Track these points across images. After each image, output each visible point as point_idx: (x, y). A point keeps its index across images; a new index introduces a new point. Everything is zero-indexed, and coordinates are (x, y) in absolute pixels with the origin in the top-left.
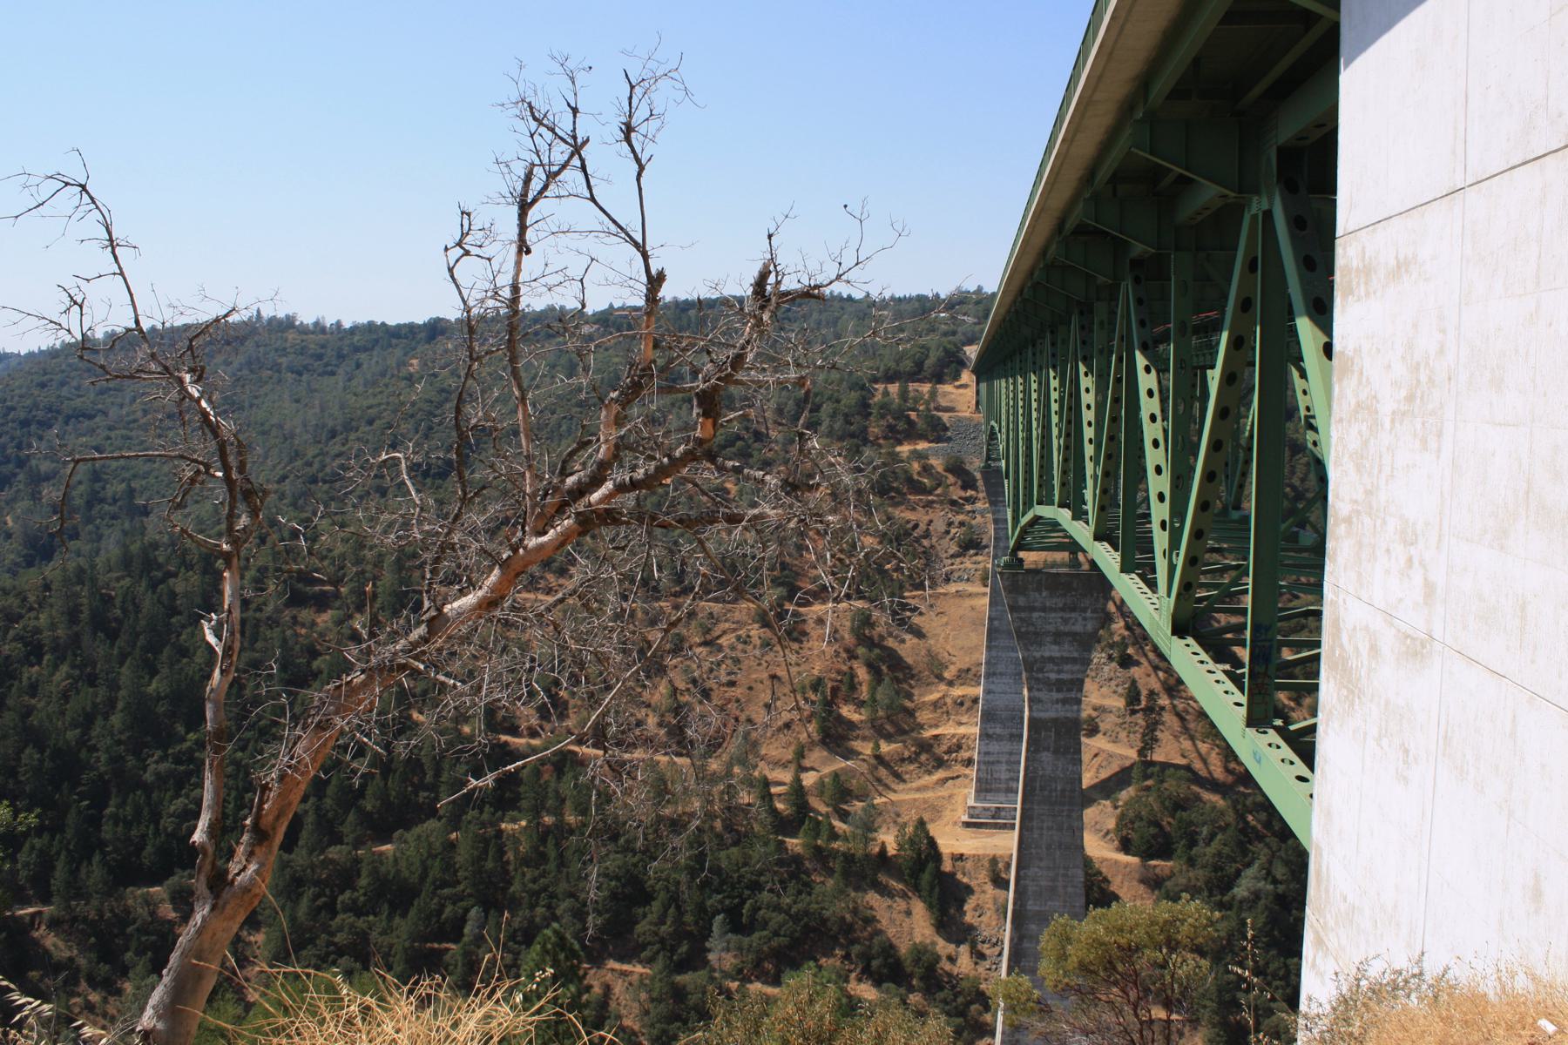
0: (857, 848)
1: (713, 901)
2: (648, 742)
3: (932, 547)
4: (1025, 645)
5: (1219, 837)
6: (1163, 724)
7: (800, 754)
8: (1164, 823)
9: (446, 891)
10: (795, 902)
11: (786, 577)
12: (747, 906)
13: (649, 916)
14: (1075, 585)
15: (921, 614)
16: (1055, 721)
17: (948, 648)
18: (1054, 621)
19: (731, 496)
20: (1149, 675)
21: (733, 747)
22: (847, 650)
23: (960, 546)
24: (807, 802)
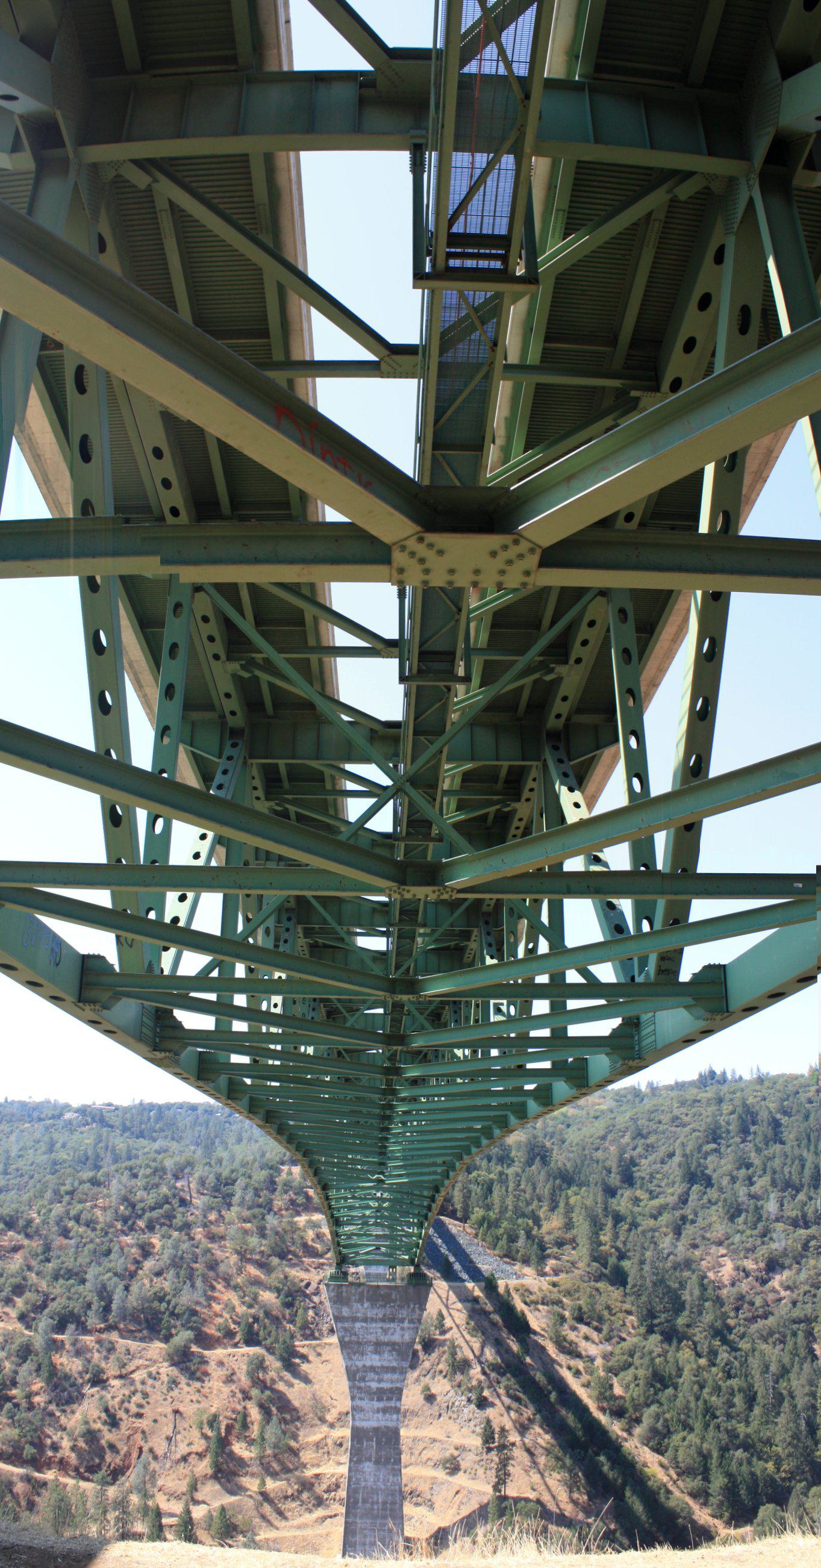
2: (63, 1465)
3: (321, 1303)
4: (348, 1354)
7: (194, 1487)
11: (195, 1322)
14: (393, 1296)
15: (308, 1361)
16: (376, 1430)
18: (374, 1332)
21: (132, 1477)
22: (243, 1392)
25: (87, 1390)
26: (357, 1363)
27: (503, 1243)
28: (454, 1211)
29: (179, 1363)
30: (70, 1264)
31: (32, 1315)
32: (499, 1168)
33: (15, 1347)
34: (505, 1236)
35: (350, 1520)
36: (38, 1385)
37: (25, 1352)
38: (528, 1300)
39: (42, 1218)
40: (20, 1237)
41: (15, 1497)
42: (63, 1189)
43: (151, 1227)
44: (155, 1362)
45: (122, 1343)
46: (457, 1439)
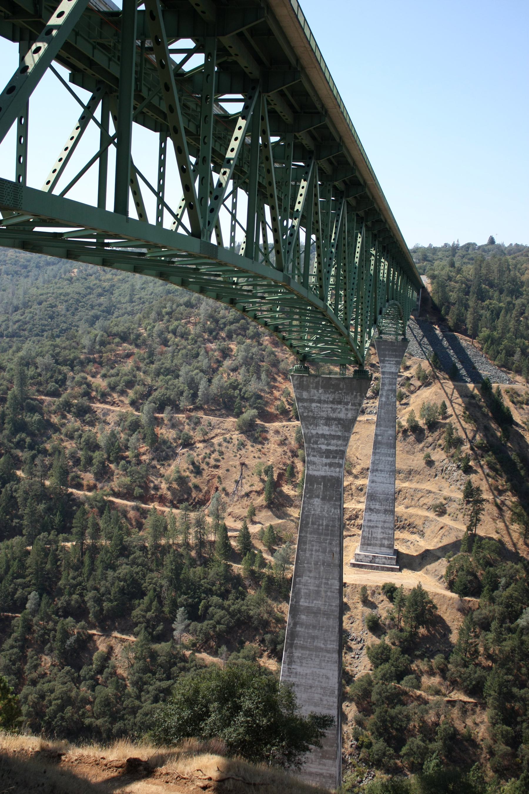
0: (275, 573)
1: (182, 599)
2: (162, 500)
4: (306, 425)
5: (513, 585)
6: (483, 510)
7: (253, 513)
8: (479, 574)
9: (19, 581)
10: (233, 604)
11: (259, 403)
12: (202, 603)
13: (142, 605)
14: (341, 386)
16: (324, 477)
17: (357, 454)
18: (326, 410)
19: (233, 353)
20: (482, 480)
22: (292, 451)
23: (374, 392)
24: (251, 542)
25: (180, 450)
26: (313, 431)
27: (503, 355)
28: (466, 330)
29: (247, 431)
30: (168, 364)
31: (141, 401)
32: (509, 299)
33: (127, 423)
34: (504, 351)
35: (303, 535)
36: (144, 448)
37: (135, 426)
38: (515, 400)
39: (148, 332)
40: (131, 347)
41: (128, 520)
42: (164, 310)
43: (230, 337)
44: (229, 431)
45: (206, 418)
46: (446, 493)
